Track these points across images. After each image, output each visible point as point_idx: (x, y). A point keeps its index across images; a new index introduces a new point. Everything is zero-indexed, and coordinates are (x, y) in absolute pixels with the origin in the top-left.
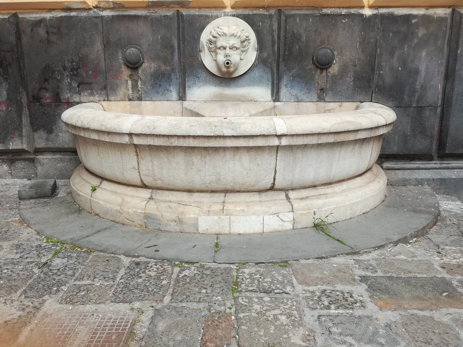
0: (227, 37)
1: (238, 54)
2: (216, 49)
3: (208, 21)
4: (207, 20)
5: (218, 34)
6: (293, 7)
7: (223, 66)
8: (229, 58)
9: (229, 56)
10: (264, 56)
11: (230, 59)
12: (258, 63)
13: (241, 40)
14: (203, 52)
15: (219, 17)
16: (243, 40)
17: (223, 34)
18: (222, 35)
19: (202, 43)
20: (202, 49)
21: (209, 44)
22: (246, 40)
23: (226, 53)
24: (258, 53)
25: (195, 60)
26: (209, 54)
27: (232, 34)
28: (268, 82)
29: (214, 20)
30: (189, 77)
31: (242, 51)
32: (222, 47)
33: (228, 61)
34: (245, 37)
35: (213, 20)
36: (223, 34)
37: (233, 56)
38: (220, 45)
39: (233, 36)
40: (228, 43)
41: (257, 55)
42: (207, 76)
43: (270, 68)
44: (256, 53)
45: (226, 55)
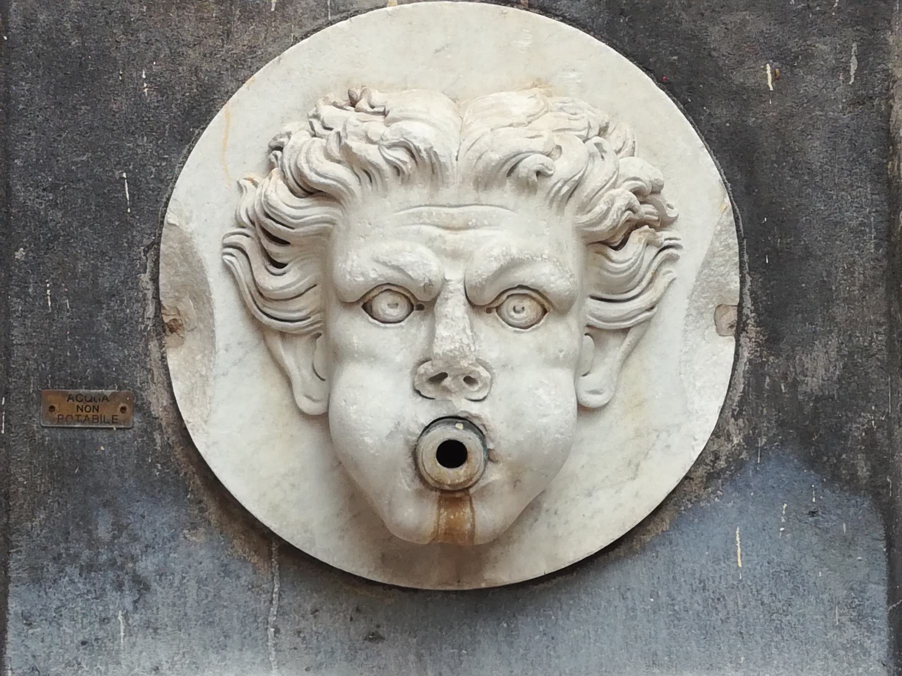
0: (447, 194)
1: (556, 362)
2: (322, 310)
3: (252, 49)
4: (243, 38)
5: (349, 158)
6: (534, 115)
7: (405, 483)
8: (462, 405)
9: (469, 380)
10: (812, 383)
11: (474, 409)
12: (750, 442)
13: (585, 218)
14: (192, 341)
15: (357, 13)
16: (608, 223)
17: (408, 165)
18: (398, 170)
19: (188, 254)
20: (187, 305)
21: (258, 261)
22: (638, 225)
23: (440, 348)
24: (746, 354)
25: (106, 412)
26: (257, 358)
27: (496, 157)
28: (851, 631)
29: (306, 36)
30: (37, 578)
31: (593, 331)
32: (388, 287)
33: (456, 432)
34: (623, 196)
35: (296, 40)
36: (408, 165)
37: (503, 382)
38: (375, 273)
39: (509, 184)
40: (455, 255)
41: (742, 368)
42: (226, 571)
43: (877, 495)
44: (727, 347)
45: (429, 369)
